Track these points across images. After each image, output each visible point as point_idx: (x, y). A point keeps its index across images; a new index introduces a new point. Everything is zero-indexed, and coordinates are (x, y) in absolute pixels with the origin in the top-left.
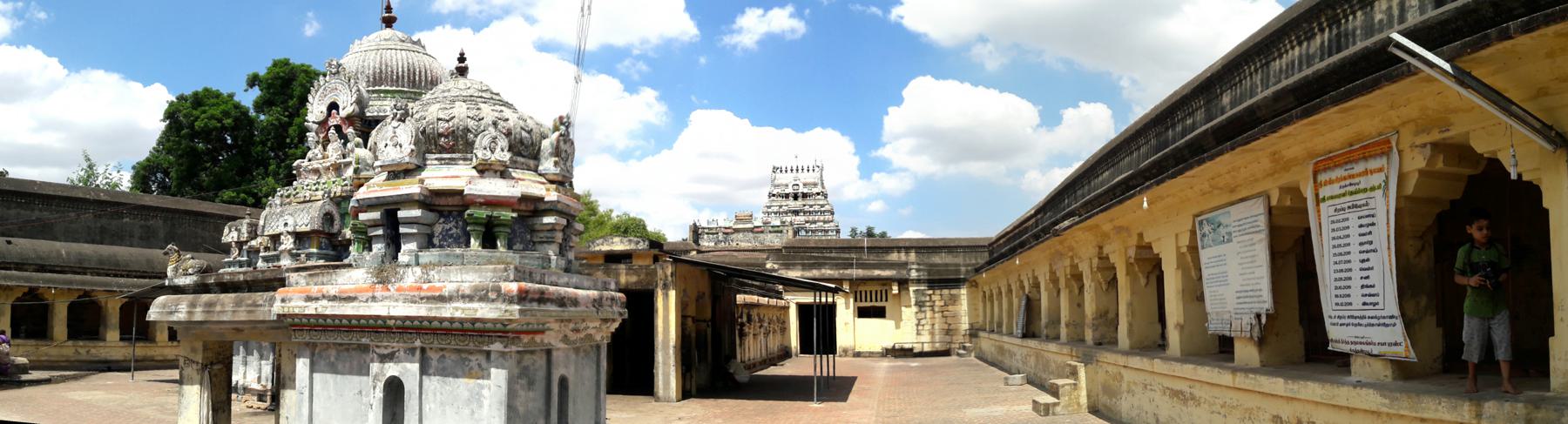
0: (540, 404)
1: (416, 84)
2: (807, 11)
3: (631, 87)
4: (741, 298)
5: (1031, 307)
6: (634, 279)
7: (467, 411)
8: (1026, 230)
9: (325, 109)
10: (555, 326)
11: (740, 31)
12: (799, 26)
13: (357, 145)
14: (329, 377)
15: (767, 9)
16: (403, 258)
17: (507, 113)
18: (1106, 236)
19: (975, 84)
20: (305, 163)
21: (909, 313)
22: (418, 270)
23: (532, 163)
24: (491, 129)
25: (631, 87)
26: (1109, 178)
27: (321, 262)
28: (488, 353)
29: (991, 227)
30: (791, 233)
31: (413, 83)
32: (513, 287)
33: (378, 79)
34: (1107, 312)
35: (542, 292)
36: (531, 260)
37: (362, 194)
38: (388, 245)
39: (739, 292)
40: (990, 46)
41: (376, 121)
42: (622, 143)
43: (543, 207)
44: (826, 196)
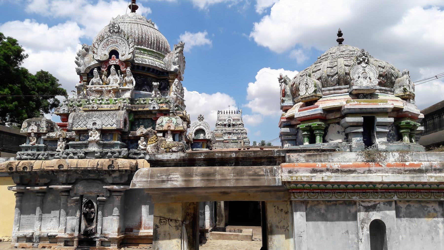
7: (429, 238)
9: (107, 54)
31: (158, 48)
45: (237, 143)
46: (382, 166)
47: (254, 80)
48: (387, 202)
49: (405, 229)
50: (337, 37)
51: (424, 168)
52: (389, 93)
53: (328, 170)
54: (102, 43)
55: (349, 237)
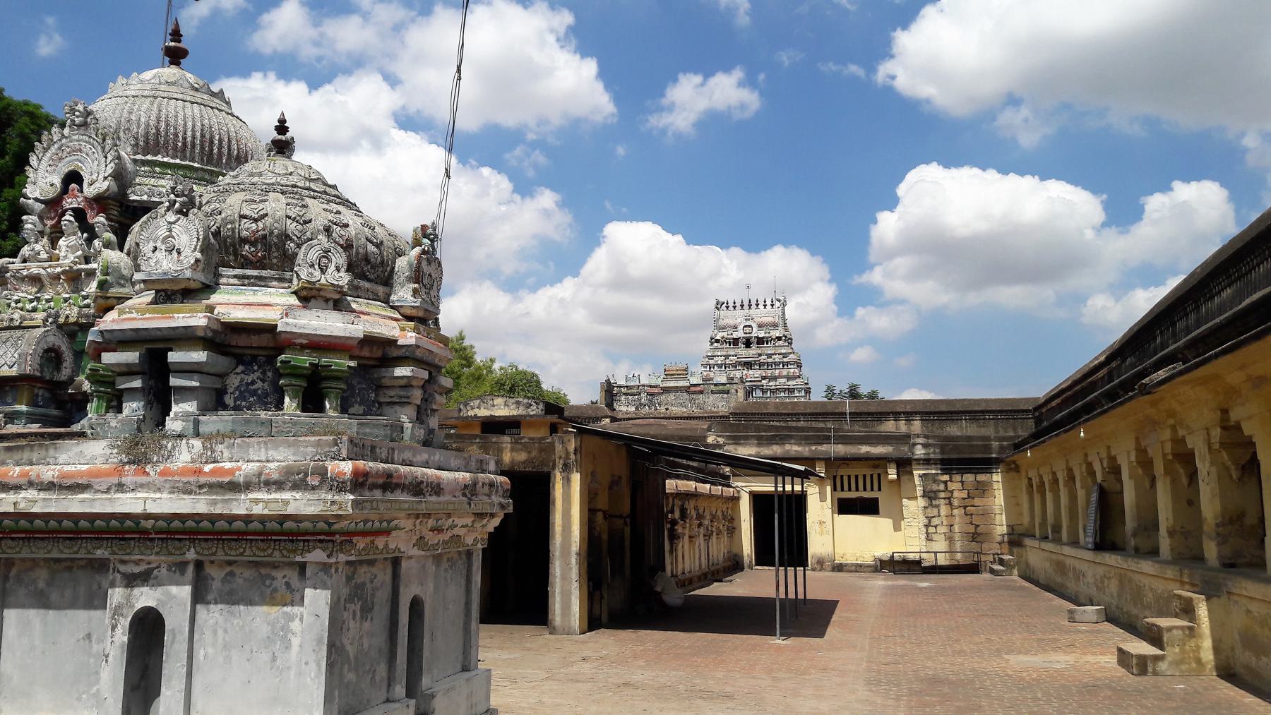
0: (380, 640)
1: (213, 157)
2: (762, 77)
3: (524, 188)
4: (671, 485)
5: (1108, 504)
6: (522, 456)
7: (265, 657)
8: (1093, 387)
9: (57, 180)
10: (407, 524)
11: (671, 108)
12: (751, 99)
13: (107, 245)
14: (34, 615)
15: (708, 75)
16: (173, 424)
17: (347, 216)
18: (1233, 393)
19: (1004, 171)
20: (16, 264)
21: (914, 508)
22: (197, 444)
23: (381, 290)
24: (322, 238)
25: (524, 188)
26: (1230, 302)
27: (35, 428)
28: (302, 567)
29: (1037, 383)
30: (741, 394)
31: (208, 157)
32: (347, 467)
33: (152, 143)
34: (1241, 516)
35: (389, 475)
36: (375, 429)
37: (111, 321)
38: (149, 405)
39: (670, 476)
40: (1025, 112)
41: (145, 208)
42: (508, 268)
43: (395, 353)
44: (789, 341)
45: (728, 392)
46: (148, 474)
47: (891, 202)
48: (176, 564)
49: (215, 632)
50: (274, 135)
51: (241, 480)
52: (274, 283)
53: (31, 484)
54: (48, 155)
55: (91, 648)
